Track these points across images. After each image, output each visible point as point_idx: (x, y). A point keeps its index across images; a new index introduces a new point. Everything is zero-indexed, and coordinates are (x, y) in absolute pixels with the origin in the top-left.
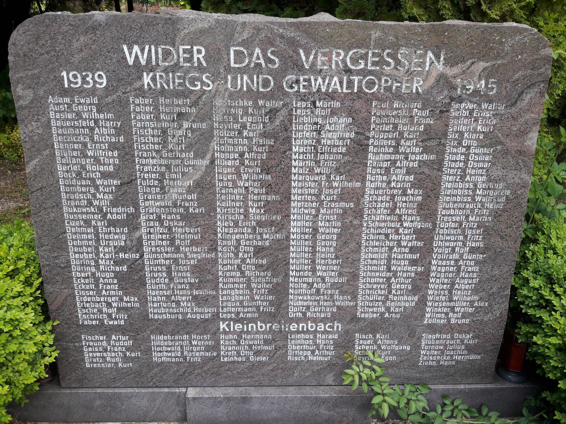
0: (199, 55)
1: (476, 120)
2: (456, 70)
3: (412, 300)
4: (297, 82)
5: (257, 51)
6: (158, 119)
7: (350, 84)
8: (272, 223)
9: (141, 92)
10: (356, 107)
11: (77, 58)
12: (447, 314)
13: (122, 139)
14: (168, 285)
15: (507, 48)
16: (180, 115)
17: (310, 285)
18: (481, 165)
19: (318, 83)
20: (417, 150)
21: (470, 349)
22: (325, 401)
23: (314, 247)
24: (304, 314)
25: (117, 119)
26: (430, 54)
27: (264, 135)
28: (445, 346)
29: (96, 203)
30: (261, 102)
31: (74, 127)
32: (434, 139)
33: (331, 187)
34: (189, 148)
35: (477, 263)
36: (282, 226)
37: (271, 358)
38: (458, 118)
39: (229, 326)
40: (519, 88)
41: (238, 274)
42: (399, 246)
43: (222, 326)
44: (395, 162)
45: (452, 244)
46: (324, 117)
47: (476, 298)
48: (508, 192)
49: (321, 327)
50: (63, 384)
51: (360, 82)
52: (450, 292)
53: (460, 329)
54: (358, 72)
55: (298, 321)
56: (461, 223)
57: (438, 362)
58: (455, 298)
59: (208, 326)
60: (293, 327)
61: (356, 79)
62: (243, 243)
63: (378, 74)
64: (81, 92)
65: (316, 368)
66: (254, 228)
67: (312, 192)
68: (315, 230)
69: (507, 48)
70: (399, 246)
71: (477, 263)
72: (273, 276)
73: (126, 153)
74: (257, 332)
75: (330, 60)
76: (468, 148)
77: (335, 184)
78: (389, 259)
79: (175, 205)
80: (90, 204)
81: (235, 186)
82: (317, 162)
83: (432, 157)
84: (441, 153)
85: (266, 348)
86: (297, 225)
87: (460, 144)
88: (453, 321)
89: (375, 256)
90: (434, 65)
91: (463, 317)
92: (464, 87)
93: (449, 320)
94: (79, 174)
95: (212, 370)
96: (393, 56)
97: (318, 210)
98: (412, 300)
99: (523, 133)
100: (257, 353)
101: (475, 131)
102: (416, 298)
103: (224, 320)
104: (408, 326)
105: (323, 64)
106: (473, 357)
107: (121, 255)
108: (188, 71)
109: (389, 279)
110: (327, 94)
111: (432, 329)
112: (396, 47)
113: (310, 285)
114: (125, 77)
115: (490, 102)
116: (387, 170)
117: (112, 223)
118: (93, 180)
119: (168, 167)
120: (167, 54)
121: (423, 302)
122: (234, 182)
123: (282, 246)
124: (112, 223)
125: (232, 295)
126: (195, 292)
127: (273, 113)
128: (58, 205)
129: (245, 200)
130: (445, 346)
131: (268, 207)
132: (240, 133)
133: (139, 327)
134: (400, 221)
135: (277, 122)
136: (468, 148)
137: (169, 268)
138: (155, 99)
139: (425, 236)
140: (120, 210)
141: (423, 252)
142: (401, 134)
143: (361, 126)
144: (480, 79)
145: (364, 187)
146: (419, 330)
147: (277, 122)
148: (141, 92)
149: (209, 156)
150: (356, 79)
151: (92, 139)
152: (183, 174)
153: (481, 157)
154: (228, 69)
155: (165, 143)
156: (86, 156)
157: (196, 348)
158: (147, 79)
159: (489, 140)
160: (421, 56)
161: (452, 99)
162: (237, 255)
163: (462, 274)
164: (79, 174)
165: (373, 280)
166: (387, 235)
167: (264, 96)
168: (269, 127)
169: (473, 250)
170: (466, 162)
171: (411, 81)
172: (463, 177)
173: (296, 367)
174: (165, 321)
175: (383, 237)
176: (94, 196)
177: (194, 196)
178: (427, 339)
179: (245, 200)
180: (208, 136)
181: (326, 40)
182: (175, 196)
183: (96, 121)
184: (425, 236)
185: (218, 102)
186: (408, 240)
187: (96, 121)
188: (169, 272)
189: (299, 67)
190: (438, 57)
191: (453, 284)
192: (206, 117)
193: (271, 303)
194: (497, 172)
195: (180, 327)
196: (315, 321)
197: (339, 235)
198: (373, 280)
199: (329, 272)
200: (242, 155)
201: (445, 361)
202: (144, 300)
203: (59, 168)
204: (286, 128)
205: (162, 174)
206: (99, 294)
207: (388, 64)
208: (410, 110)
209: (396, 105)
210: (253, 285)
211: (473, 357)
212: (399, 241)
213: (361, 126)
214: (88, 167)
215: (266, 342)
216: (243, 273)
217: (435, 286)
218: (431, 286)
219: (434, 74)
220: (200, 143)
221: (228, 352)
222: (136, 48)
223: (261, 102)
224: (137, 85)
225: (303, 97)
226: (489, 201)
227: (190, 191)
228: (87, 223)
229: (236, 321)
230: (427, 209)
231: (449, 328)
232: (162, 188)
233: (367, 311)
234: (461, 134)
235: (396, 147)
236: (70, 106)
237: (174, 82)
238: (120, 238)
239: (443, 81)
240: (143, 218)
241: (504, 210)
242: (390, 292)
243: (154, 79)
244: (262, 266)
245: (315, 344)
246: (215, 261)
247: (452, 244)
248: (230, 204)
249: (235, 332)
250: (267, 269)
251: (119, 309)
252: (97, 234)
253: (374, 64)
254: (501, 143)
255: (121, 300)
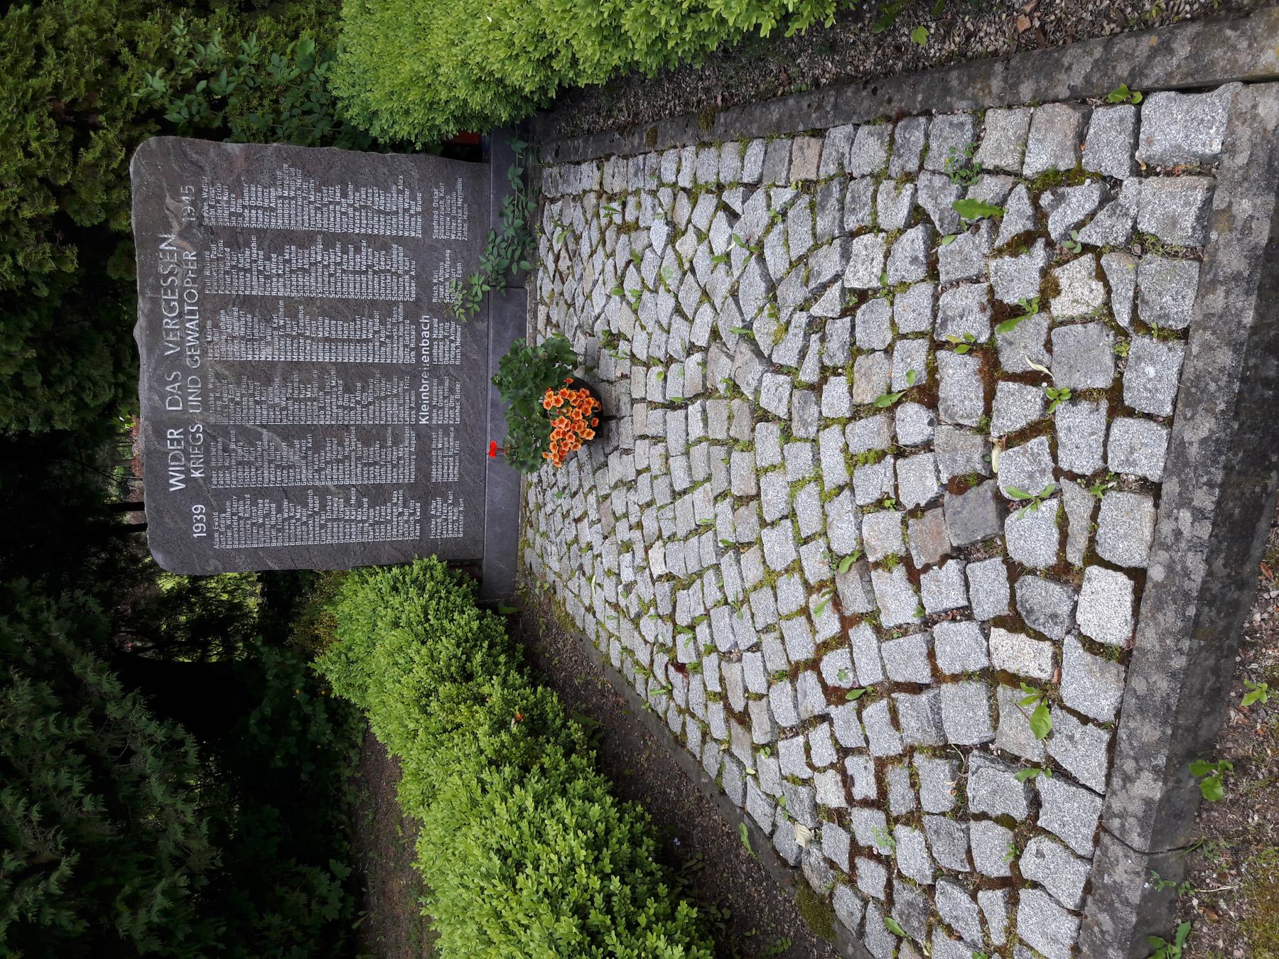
0: (173, 434)
1: (218, 202)
2: (175, 223)
3: (397, 251)
4: (191, 356)
5: (168, 388)
6: (229, 468)
7: (192, 313)
8: (321, 378)
9: (207, 479)
10: (211, 307)
11: (183, 526)
12: (411, 216)
13: (247, 496)
14: (381, 467)
15: (152, 179)
16: (225, 450)
17: (382, 344)
18: (260, 194)
19: (191, 339)
20: (248, 252)
21: (450, 189)
22: (498, 333)
23: (343, 341)
24: (412, 349)
25: (230, 498)
26: (163, 246)
27: (239, 384)
28: (446, 215)
29: (304, 519)
30: (210, 386)
31: (239, 531)
32: (237, 238)
33: (284, 326)
34: (255, 446)
35: (356, 190)
36: (323, 368)
37: (457, 379)
38: (217, 218)
39: (423, 416)
40: (187, 165)
41: (371, 407)
42: (341, 264)
43: (424, 421)
44: (259, 271)
45: (338, 215)
46: (221, 333)
47: (394, 188)
48: (285, 166)
49: (425, 334)
50: (479, 556)
51: (190, 305)
52: (388, 214)
53: (427, 201)
54: (181, 306)
55: (419, 355)
56: (317, 208)
57: (464, 221)
58: (394, 208)
59: (424, 436)
60: (426, 359)
61: (187, 308)
62: (340, 403)
63: (183, 289)
64: (209, 524)
65: (469, 338)
66: (326, 393)
67: (289, 343)
68: (326, 339)
69: (152, 179)
70: (341, 264)
71: (356, 190)
72: (374, 377)
73: (260, 493)
74: (431, 391)
75: (172, 330)
76: (244, 207)
77: (282, 322)
78: (354, 273)
79: (306, 458)
80: (306, 523)
81: (286, 408)
82: (261, 338)
83: (254, 238)
84: (250, 231)
85: (447, 384)
86: (324, 356)
87: (241, 215)
88: (419, 209)
89: (351, 285)
90: (170, 242)
91: (414, 199)
92: (189, 215)
93: (417, 213)
94: (278, 530)
95: (467, 431)
96: (166, 278)
97: (307, 338)
98: (397, 251)
99: (228, 157)
100: (452, 391)
101: (228, 202)
102: (395, 246)
103: (417, 420)
104: (424, 253)
105: (175, 335)
106: (459, 186)
107: (353, 502)
108: (187, 442)
109: (375, 272)
110: (200, 332)
111: (427, 229)
112: (158, 276)
113: (382, 344)
114: (195, 491)
115: (201, 190)
116: (266, 277)
117: (323, 507)
118: (284, 520)
119: (270, 462)
120: (175, 458)
121: (399, 240)
122: (282, 409)
123: (344, 370)
124: (323, 507)
125: (394, 412)
126: (389, 443)
127: (218, 376)
128: (308, 548)
129: (299, 400)
130: (446, 215)
131: (305, 382)
132: (237, 403)
133: (423, 491)
134: (316, 264)
135: (227, 373)
136: (244, 207)
137: (365, 465)
138: (212, 469)
139: (330, 240)
140: (310, 501)
141: (348, 241)
142: (233, 267)
143: (226, 302)
144: (181, 201)
145: (283, 298)
146: (428, 242)
147: (227, 373)
148: (207, 479)
149: (259, 429)
150: (187, 308)
151: (247, 519)
152: (276, 450)
153: (253, 195)
154: (184, 411)
155: (250, 464)
156: (264, 524)
157: (445, 445)
158: (197, 474)
159: (236, 189)
160: (164, 254)
161: (200, 225)
162: (352, 409)
163: (369, 203)
164: (278, 530)
165: (377, 287)
166: (330, 275)
167: (205, 384)
168: (232, 379)
169: (344, 195)
170: (257, 208)
171: (187, 262)
172: (272, 210)
173: (467, 357)
174: (417, 469)
175: (332, 279)
176: (298, 520)
177: (296, 442)
178: (438, 233)
179: (299, 400)
180: (242, 430)
181: (155, 327)
182: (297, 458)
183: (233, 514)
184: (330, 240)
185: (212, 420)
186: (335, 256)
187: (233, 514)
188: (369, 465)
189: (180, 354)
190: (165, 239)
191: (379, 212)
192: (225, 431)
193: (401, 378)
194: (266, 178)
195: (424, 456)
196: (419, 338)
197: (331, 318)
198: (377, 287)
199: (369, 326)
200: (257, 402)
201: (463, 215)
202: (398, 486)
203: (274, 545)
204: (230, 365)
205: (277, 467)
206: (387, 522)
207: (173, 281)
208: (212, 260)
209: (208, 273)
210: (383, 394)
211: (459, 186)
212: (336, 264)
213: (226, 302)
214: (273, 523)
215: (441, 383)
216: (370, 404)
217: (381, 228)
218: (382, 232)
219: (179, 242)
220: (249, 436)
221: (451, 415)
222: (172, 481)
223: (210, 386)
224: (201, 482)
225: (204, 353)
226: (293, 183)
227: (291, 445)
228: (322, 526)
229: (418, 409)
230: (304, 240)
231: (427, 213)
232: (290, 467)
233: (410, 291)
234: (231, 214)
235: (245, 271)
236: (221, 533)
237: (196, 453)
238: (337, 503)
239: (185, 234)
240: (317, 483)
241: (303, 168)
242: (389, 271)
243: (196, 469)
244: (363, 387)
245: (443, 339)
246: (357, 427)
247: (338, 215)
248: (303, 413)
249: (430, 412)
250: (367, 382)
251: (405, 506)
252: (333, 520)
253: (173, 294)
254: (239, 177)
255: (396, 504)
